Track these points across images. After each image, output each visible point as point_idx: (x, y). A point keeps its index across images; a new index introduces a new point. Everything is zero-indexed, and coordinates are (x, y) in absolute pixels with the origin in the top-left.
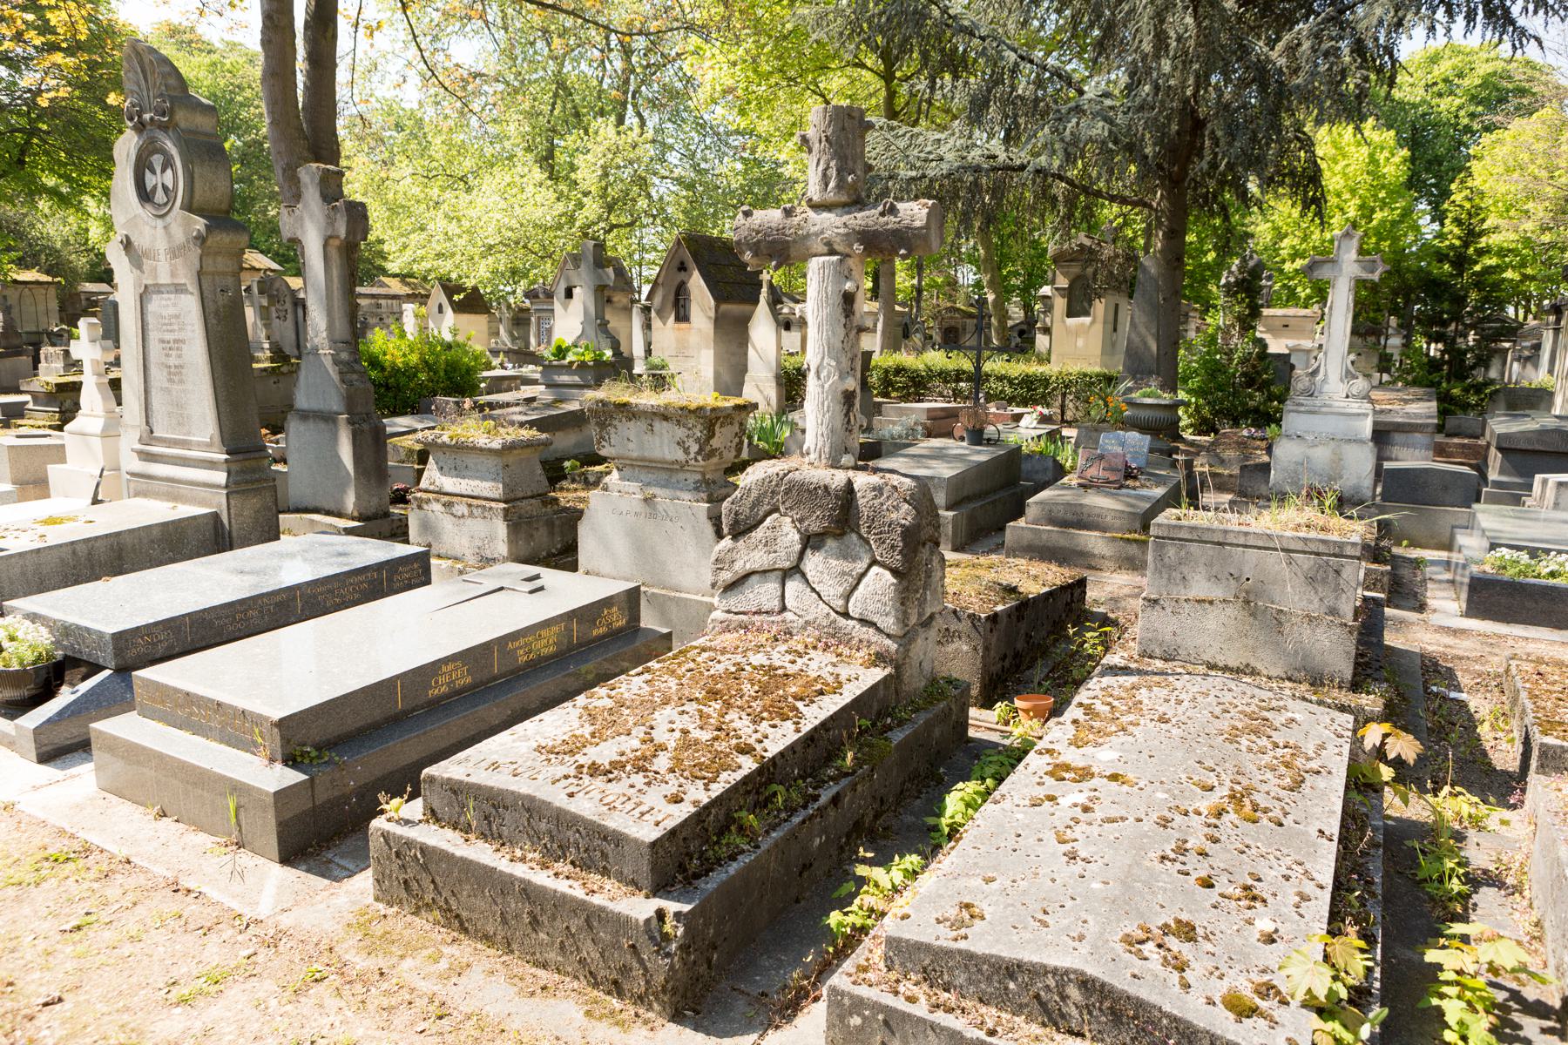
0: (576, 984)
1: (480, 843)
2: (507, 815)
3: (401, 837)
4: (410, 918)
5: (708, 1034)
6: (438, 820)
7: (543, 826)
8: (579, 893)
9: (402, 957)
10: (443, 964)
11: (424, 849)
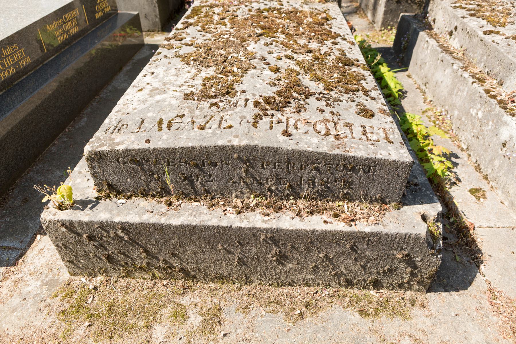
0: (329, 291)
1: (185, 204)
2: (216, 172)
3: (90, 224)
4: (123, 282)
5: (457, 290)
6: (118, 193)
7: (267, 171)
8: (340, 226)
9: (148, 327)
10: (195, 319)
11: (126, 228)
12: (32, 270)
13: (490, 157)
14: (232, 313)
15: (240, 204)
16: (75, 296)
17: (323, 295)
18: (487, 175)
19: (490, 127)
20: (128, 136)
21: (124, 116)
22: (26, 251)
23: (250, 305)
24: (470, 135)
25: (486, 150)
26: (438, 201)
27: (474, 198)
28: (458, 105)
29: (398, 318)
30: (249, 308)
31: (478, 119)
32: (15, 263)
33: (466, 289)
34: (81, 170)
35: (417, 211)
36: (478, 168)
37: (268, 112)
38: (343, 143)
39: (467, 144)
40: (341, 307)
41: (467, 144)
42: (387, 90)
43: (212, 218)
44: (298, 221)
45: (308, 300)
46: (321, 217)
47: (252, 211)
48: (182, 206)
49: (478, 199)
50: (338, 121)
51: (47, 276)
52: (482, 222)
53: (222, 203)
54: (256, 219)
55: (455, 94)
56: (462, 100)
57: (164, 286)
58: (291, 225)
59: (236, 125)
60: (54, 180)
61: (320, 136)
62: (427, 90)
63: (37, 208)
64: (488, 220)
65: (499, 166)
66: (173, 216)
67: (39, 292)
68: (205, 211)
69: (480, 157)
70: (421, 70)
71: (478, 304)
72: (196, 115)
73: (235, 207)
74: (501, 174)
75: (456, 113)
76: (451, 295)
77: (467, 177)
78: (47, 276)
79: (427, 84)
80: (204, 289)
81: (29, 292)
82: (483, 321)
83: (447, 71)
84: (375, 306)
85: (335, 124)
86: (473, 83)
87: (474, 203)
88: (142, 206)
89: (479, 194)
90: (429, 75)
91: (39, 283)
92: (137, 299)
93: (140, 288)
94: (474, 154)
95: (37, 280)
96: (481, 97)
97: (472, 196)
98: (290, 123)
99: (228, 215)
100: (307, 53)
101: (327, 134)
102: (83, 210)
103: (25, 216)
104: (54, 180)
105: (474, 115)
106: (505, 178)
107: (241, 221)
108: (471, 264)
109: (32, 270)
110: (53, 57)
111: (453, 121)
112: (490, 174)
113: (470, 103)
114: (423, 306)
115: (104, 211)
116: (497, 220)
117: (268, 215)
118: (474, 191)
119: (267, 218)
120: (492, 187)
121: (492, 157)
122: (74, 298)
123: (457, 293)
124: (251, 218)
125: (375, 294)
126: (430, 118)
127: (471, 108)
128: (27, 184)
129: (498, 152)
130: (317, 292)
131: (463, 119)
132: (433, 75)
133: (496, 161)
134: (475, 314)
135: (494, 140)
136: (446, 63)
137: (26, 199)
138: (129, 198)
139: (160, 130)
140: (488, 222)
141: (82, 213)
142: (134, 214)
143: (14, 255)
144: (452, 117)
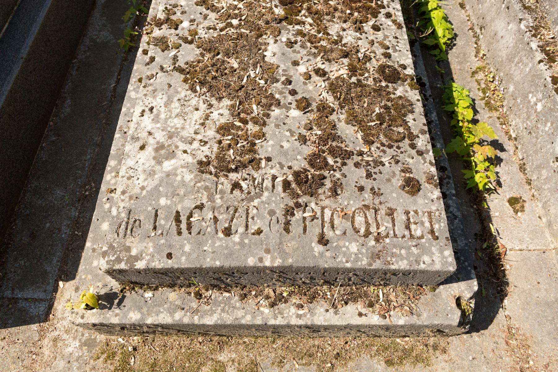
12: (67, 326)
13: (539, 162)
14: (268, 368)
15: (272, 294)
16: (117, 358)
17: (352, 346)
18: (531, 180)
19: (547, 129)
20: (145, 244)
21: (132, 202)
22: (53, 303)
23: (284, 358)
24: (523, 124)
25: (536, 152)
26: (475, 276)
27: (512, 210)
28: (516, 79)
29: (420, 365)
30: (284, 362)
31: (536, 111)
32: (46, 319)
33: (487, 328)
34: (95, 246)
35: (452, 292)
36: (522, 168)
37: (300, 200)
38: (384, 247)
39: (516, 132)
40: (369, 356)
41: (516, 132)
42: (433, 40)
43: (246, 314)
44: (332, 314)
45: (338, 351)
46: (355, 306)
47: (286, 302)
48: (212, 298)
49: (516, 212)
50: (380, 206)
51: (83, 335)
52: (515, 244)
53: (253, 293)
54: (291, 314)
55: (515, 62)
56: (522, 75)
57: (200, 343)
58: (325, 320)
59: (265, 229)
60: (56, 202)
61: (358, 238)
62: (481, 37)
63: (49, 246)
64: (521, 241)
65: (546, 178)
66: (206, 313)
67: (80, 354)
68: (238, 304)
69: (527, 156)
70: (478, 4)
71: (495, 345)
72: (217, 205)
73: (267, 297)
74: (546, 188)
75: (512, 88)
76: (472, 337)
77: (508, 181)
78: (83, 335)
79: (483, 29)
80: (239, 344)
81: (71, 354)
82: (497, 363)
83: (511, 25)
84: (400, 354)
85: (376, 212)
86: (540, 61)
87: (510, 217)
88: (171, 300)
89: (518, 206)
90: (488, 18)
91: (78, 344)
92: (177, 358)
93: (178, 347)
94: (522, 149)
95: (75, 339)
96: (545, 86)
97: (510, 207)
98: (326, 219)
99: (262, 309)
100: (342, 58)
101: (367, 234)
102: (110, 308)
103: (40, 257)
104: (56, 202)
105: (532, 103)
106: (549, 194)
107: (275, 318)
108: (495, 297)
109: (67, 326)
110: (7, 24)
111: (506, 96)
112: (534, 180)
113: (531, 85)
114: (444, 351)
115: (133, 309)
116: (531, 241)
117: (302, 307)
118: (513, 201)
119: (301, 312)
120: (533, 196)
121: (541, 164)
122: (116, 360)
123: (477, 334)
124: (285, 312)
125: (400, 342)
126: (479, 84)
127: (530, 92)
128: (28, 212)
129: (548, 162)
130: (346, 343)
131: (519, 101)
132: (493, 20)
133: (545, 171)
134: (491, 356)
135: (548, 147)
136: (513, 15)
137: (33, 233)
138: (156, 289)
139: (180, 233)
140: (521, 244)
141: (110, 313)
142: (165, 312)
143: (42, 309)
144: (505, 90)
